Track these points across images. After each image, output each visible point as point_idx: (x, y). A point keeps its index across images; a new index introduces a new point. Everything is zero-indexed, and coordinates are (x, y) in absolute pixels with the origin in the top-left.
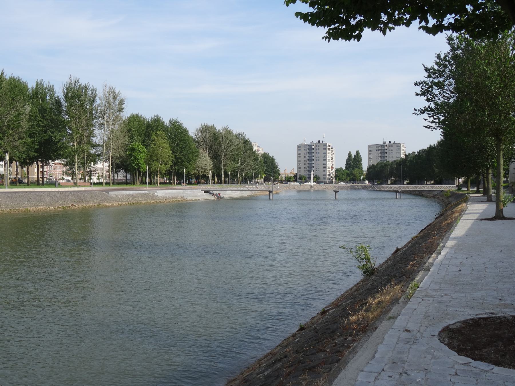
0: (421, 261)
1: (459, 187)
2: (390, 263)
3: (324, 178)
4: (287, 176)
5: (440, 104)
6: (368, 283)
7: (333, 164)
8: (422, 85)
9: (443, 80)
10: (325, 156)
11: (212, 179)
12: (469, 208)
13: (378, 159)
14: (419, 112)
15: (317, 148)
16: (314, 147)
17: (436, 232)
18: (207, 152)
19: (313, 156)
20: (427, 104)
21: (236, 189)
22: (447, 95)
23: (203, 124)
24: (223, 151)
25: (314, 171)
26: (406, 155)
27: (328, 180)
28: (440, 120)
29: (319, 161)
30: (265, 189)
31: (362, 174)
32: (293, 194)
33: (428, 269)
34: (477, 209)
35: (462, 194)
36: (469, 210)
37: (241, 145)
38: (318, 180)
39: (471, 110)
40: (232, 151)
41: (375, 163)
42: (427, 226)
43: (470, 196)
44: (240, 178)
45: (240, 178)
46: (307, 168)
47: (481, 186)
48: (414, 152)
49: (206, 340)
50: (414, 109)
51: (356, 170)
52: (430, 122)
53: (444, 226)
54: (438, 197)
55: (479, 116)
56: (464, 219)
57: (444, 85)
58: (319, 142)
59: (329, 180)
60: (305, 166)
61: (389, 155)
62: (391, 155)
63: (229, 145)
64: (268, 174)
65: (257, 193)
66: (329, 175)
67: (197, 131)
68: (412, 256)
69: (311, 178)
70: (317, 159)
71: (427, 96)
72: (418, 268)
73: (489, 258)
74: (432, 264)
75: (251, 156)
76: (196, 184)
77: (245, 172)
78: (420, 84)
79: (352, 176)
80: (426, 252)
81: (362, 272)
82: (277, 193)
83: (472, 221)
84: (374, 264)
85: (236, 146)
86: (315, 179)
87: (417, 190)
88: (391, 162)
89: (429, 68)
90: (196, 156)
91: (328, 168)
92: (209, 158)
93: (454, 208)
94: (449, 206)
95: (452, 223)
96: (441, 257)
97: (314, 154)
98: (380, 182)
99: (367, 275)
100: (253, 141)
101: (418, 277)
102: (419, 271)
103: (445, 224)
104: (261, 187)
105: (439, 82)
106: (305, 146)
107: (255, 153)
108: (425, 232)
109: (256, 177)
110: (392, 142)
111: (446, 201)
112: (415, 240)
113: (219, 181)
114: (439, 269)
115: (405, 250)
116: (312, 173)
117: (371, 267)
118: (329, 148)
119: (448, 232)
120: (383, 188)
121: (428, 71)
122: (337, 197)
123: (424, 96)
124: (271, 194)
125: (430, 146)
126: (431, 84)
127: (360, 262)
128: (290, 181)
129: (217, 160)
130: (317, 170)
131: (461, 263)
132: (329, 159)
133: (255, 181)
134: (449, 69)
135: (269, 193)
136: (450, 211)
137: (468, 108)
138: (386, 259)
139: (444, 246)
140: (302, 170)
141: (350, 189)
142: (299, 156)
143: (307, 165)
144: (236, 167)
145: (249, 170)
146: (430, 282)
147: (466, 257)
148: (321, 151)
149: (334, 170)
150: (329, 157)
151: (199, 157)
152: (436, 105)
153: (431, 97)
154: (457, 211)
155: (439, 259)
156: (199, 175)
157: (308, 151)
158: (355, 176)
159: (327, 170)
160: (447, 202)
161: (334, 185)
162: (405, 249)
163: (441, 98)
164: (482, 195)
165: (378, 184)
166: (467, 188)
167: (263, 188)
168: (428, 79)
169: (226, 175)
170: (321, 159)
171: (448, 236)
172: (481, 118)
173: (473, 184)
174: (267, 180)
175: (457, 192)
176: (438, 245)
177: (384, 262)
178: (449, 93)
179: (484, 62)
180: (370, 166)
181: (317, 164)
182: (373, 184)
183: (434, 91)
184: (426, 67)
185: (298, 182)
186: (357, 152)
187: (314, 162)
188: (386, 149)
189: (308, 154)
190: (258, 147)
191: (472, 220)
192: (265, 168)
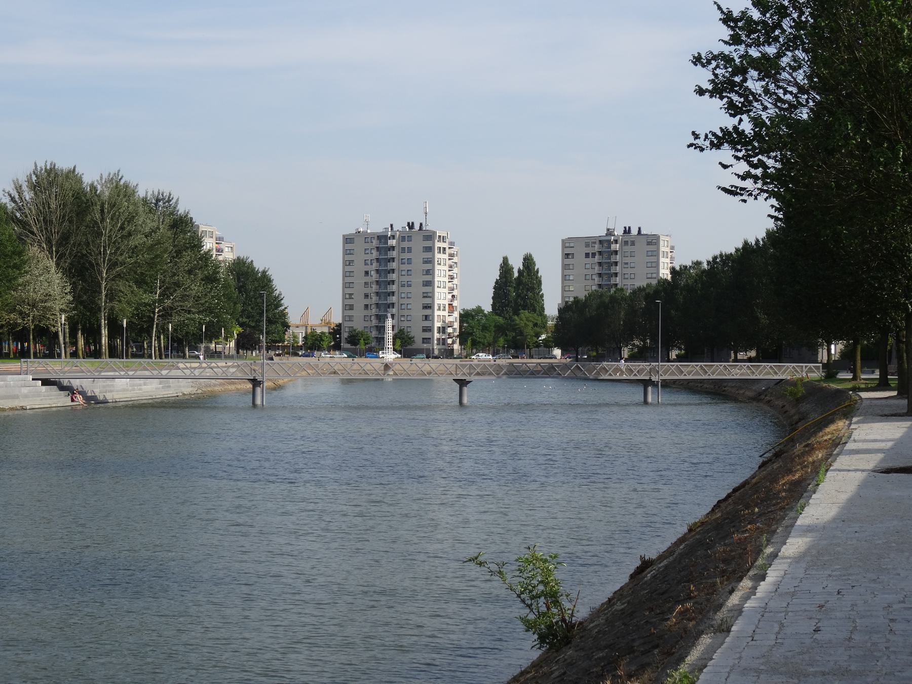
0: (708, 600)
1: (831, 370)
2: (619, 606)
3: (427, 340)
4: (309, 331)
5: (768, 123)
6: (552, 673)
7: (453, 296)
8: (714, 64)
9: (775, 51)
10: (430, 272)
11: (67, 340)
12: (856, 435)
13: (590, 282)
14: (707, 143)
15: (406, 244)
16: (394, 241)
17: (757, 510)
18: (51, 253)
19: (393, 271)
20: (730, 122)
21: (147, 373)
22: (788, 97)
23: (41, 164)
24: (105, 250)
25: (396, 317)
26: (673, 271)
27: (440, 347)
28: (769, 171)
29: (409, 286)
30: (239, 375)
31: (544, 326)
32: (328, 388)
33: (724, 627)
34: (879, 437)
35: (838, 391)
36: (855, 441)
37: (164, 230)
38: (409, 347)
39: (858, 146)
40: (134, 250)
41: (582, 295)
42: (735, 490)
43: (861, 398)
44: (159, 338)
45: (159, 338)
46: (373, 306)
47: (893, 367)
48: (698, 264)
49: (309, 631)
50: (693, 133)
51: (524, 314)
52: (739, 176)
53: (779, 492)
54: (768, 398)
55: (880, 163)
56: (839, 470)
57: (779, 69)
58: (411, 226)
59: (441, 347)
60: (367, 302)
61: (625, 271)
62: (632, 271)
63: (125, 233)
64: (250, 326)
65: (215, 385)
66: (443, 330)
67: (19, 189)
68: (685, 586)
69: (386, 340)
70: (405, 279)
71: (728, 98)
72: (698, 624)
73: (902, 589)
74: (738, 611)
75: (195, 267)
76: (15, 358)
77: (176, 319)
78: (709, 62)
79: (511, 334)
80: (723, 572)
81: (536, 637)
82: (278, 388)
83: (860, 476)
84: (570, 612)
85: (146, 236)
86: (398, 342)
87: (706, 377)
88: (629, 291)
89: (736, 14)
90: (17, 267)
91: (439, 309)
92: (60, 275)
93: (815, 433)
94: (801, 427)
95: (805, 480)
96: (764, 587)
97: (394, 265)
98: (597, 351)
99: (552, 645)
100: (203, 221)
101: (693, 656)
102: (699, 634)
103: (784, 484)
104: (229, 367)
105: (765, 56)
106: (367, 237)
107: (207, 259)
108: (726, 507)
109: (213, 334)
110: (634, 232)
111: (793, 411)
112: (698, 533)
113: (93, 348)
114: (757, 627)
115: (666, 567)
116: (389, 323)
117: (563, 620)
118: (442, 245)
119: (791, 509)
120: (607, 371)
121: (732, 24)
122: (465, 400)
123: (722, 98)
124: (258, 390)
125: (746, 243)
126: (741, 62)
127: (529, 606)
128: (320, 349)
129: (84, 280)
130: (406, 313)
131: (821, 606)
132: (442, 279)
133: (207, 349)
134: (794, 21)
135: (251, 386)
136: (801, 443)
137: (847, 138)
138: (610, 595)
139: (775, 555)
140: (359, 313)
141: (505, 374)
142: (348, 269)
143: (375, 299)
144: (146, 305)
145: (189, 312)
146: (728, 670)
147: (838, 587)
148: (417, 256)
149: (456, 314)
150: (441, 274)
151: (27, 268)
152: (756, 125)
153: (742, 100)
154: (820, 443)
155: (758, 595)
156: (25, 330)
157: (375, 254)
158: (521, 333)
159: (437, 313)
160: (794, 415)
161: (458, 361)
162: (665, 562)
163: (769, 106)
164: (895, 393)
165: (590, 359)
166: (854, 371)
167: (234, 370)
168: (733, 48)
169: (115, 329)
170: (418, 279)
171: (790, 521)
172: (884, 168)
173: (873, 358)
174: (246, 343)
175: (824, 385)
176: (759, 551)
177: (602, 604)
178: (795, 90)
179: (893, 5)
180: (567, 302)
181: (403, 295)
182: (577, 360)
183: (750, 84)
184: (725, 11)
185: (346, 350)
186: (528, 261)
187: (394, 288)
188: (616, 252)
189: (375, 265)
190: (219, 240)
191: (863, 471)
192: (239, 307)
